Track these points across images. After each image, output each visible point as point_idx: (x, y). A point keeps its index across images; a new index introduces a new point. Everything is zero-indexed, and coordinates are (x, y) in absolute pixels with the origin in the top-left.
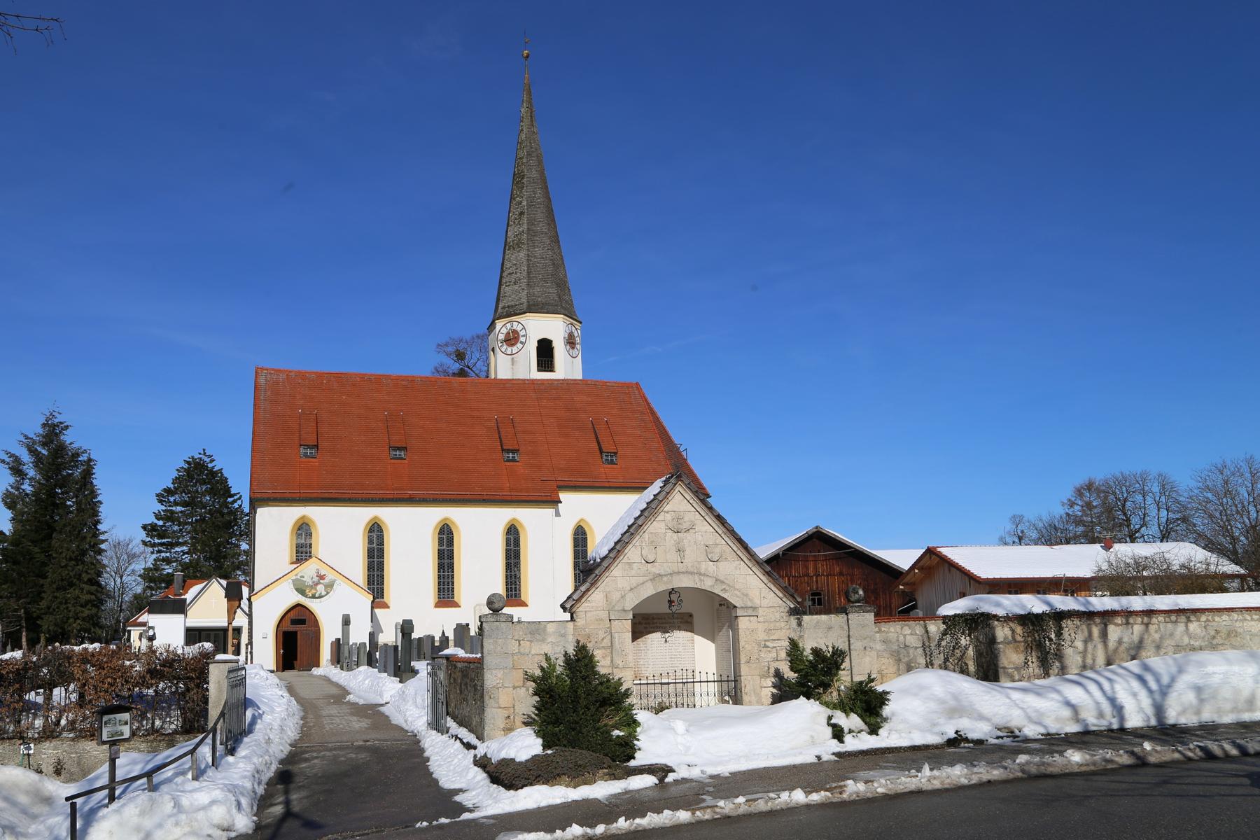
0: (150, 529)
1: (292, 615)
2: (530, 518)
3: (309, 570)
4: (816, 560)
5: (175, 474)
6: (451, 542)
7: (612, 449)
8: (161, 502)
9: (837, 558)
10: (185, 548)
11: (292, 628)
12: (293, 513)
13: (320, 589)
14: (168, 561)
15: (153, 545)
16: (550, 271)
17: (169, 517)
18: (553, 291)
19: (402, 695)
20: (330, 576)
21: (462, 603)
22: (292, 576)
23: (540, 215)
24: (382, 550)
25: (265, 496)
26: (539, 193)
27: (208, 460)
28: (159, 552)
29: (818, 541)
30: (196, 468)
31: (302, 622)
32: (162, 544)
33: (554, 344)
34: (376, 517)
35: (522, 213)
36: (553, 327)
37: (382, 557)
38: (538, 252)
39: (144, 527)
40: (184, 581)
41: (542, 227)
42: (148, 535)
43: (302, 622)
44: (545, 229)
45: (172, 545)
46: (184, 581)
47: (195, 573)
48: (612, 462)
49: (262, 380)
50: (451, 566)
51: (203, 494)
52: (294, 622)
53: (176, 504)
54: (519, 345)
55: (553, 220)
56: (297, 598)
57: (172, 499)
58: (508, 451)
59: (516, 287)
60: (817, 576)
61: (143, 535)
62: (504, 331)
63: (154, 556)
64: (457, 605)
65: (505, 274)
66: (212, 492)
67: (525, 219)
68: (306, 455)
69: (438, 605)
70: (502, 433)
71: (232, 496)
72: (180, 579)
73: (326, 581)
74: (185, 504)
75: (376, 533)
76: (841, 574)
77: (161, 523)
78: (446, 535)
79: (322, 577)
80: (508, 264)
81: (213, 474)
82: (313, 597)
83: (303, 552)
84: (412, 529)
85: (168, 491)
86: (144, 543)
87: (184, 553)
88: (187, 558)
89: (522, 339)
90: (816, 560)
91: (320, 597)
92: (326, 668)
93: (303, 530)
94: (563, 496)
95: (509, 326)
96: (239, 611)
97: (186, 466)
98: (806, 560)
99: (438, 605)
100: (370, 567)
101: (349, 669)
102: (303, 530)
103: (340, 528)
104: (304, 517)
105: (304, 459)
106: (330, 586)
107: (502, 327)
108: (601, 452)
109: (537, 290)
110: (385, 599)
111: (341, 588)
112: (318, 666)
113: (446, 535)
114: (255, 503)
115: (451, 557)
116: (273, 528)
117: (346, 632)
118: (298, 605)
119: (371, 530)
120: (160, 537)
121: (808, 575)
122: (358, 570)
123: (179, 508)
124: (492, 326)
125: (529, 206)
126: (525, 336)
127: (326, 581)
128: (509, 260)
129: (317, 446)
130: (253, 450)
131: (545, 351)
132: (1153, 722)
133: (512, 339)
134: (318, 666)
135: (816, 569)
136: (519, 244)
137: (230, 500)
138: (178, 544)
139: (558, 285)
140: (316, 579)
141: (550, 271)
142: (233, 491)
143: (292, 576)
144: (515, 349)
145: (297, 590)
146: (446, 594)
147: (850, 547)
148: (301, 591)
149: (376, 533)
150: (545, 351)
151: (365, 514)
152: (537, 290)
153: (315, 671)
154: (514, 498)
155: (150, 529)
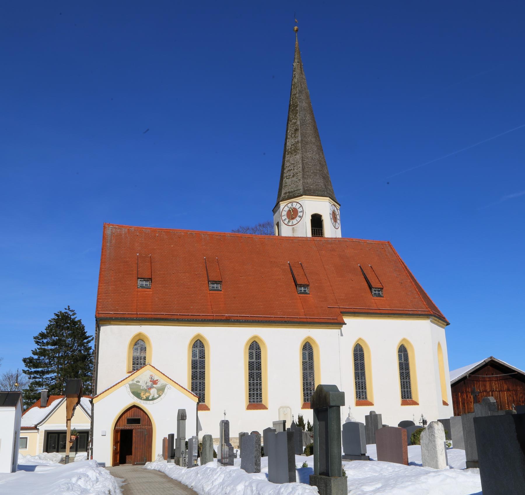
0: (29, 362)
1: (128, 415)
2: (321, 336)
3: (143, 376)
4: (490, 380)
5: (49, 323)
6: (259, 356)
7: (379, 286)
8: (37, 343)
9: (505, 379)
10: (53, 375)
11: (128, 427)
12: (132, 330)
13: (154, 392)
14: (40, 384)
15: (30, 373)
16: (318, 168)
17: (43, 353)
18: (321, 182)
19: (186, 473)
20: (162, 381)
21: (269, 406)
22: (129, 381)
23: (310, 131)
24: (204, 362)
25: (108, 316)
26: (308, 117)
27: (71, 313)
28: (35, 378)
29: (493, 367)
30: (62, 319)
31: (137, 421)
32: (36, 372)
33: (323, 218)
34: (199, 335)
35: (296, 130)
36: (322, 206)
37: (204, 367)
38: (309, 155)
39: (24, 360)
40: (48, 396)
41: (311, 139)
42: (26, 366)
43: (137, 421)
44: (313, 140)
45: (43, 373)
46: (48, 396)
47: (55, 391)
48: (379, 295)
49: (109, 232)
50: (259, 376)
51: (67, 337)
52: (131, 421)
53: (48, 344)
54: (298, 219)
55: (318, 135)
56: (133, 400)
57: (45, 341)
58: (301, 286)
59: (294, 179)
60: (493, 391)
61: (23, 366)
62: (287, 209)
63: (32, 381)
64: (264, 408)
65: (285, 171)
66: (73, 336)
67: (299, 134)
68: (142, 287)
69: (250, 407)
70: (295, 273)
71: (87, 338)
72: (46, 394)
73: (159, 385)
74: (54, 343)
75: (199, 348)
76: (508, 390)
77: (36, 357)
78: (255, 351)
79: (155, 382)
80: (287, 164)
81: (74, 323)
82: (147, 399)
83: (138, 363)
84: (226, 344)
85: (43, 336)
86: (24, 372)
87: (52, 379)
88: (53, 382)
89: (300, 214)
90: (490, 380)
91: (153, 399)
92: (158, 461)
93: (139, 345)
94: (346, 319)
95: (290, 205)
96: (78, 408)
97: (56, 317)
98: (484, 381)
99: (250, 407)
100: (194, 377)
101: (190, 465)
102: (139, 345)
103: (170, 344)
104: (140, 334)
105: (140, 289)
106: (161, 390)
107: (284, 207)
108: (370, 287)
109: (309, 181)
110: (206, 403)
111: (171, 392)
112: (150, 460)
113: (255, 351)
114: (100, 321)
115: (259, 368)
116: (113, 344)
117: (181, 428)
118: (134, 406)
119: (195, 346)
120: (36, 366)
121: (486, 391)
122: (184, 377)
123: (50, 347)
124: (277, 206)
125: (302, 125)
126: (303, 211)
127: (159, 385)
128: (289, 161)
129: (151, 279)
130: (100, 282)
131: (317, 222)
132: (325, 471)
133: (293, 214)
134: (150, 460)
135: (491, 386)
136: (295, 151)
137: (85, 341)
138: (48, 372)
139: (324, 178)
140: (150, 384)
141: (318, 168)
142: (88, 334)
143: (129, 381)
144: (295, 221)
145: (133, 393)
146: (255, 398)
147: (514, 371)
148: (137, 394)
149: (199, 348)
150: (317, 222)
151: (189, 332)
152: (309, 181)
153: (149, 466)
154: (309, 320)
155: (29, 362)
